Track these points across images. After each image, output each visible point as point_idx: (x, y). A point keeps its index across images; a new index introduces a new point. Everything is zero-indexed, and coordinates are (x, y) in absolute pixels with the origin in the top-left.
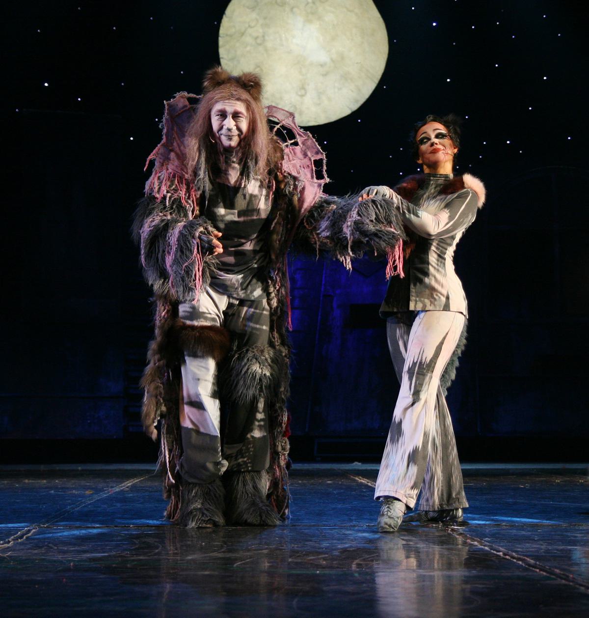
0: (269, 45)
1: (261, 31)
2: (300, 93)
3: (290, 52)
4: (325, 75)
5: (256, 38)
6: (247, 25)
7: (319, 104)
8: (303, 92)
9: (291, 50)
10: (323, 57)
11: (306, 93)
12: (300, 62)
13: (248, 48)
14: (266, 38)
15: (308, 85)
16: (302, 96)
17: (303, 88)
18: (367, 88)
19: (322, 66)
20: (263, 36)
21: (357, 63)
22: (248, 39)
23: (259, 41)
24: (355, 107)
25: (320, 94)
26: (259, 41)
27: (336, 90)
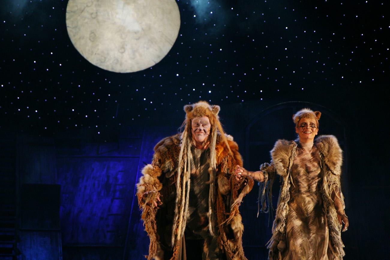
0: (100, 18)
1: (95, 9)
2: (121, 51)
3: (114, 24)
4: (138, 39)
5: (92, 14)
6: (85, 5)
7: (134, 59)
8: (123, 50)
9: (115, 22)
10: (136, 27)
11: (125, 51)
12: (121, 31)
13: (86, 20)
14: (99, 14)
15: (126, 45)
16: (122, 53)
17: (123, 47)
18: (166, 48)
19: (136, 33)
20: (97, 13)
21: (159, 32)
22: (86, 14)
23: (93, 16)
24: (158, 61)
25: (134, 52)
26: (93, 16)
27: (145, 49)
